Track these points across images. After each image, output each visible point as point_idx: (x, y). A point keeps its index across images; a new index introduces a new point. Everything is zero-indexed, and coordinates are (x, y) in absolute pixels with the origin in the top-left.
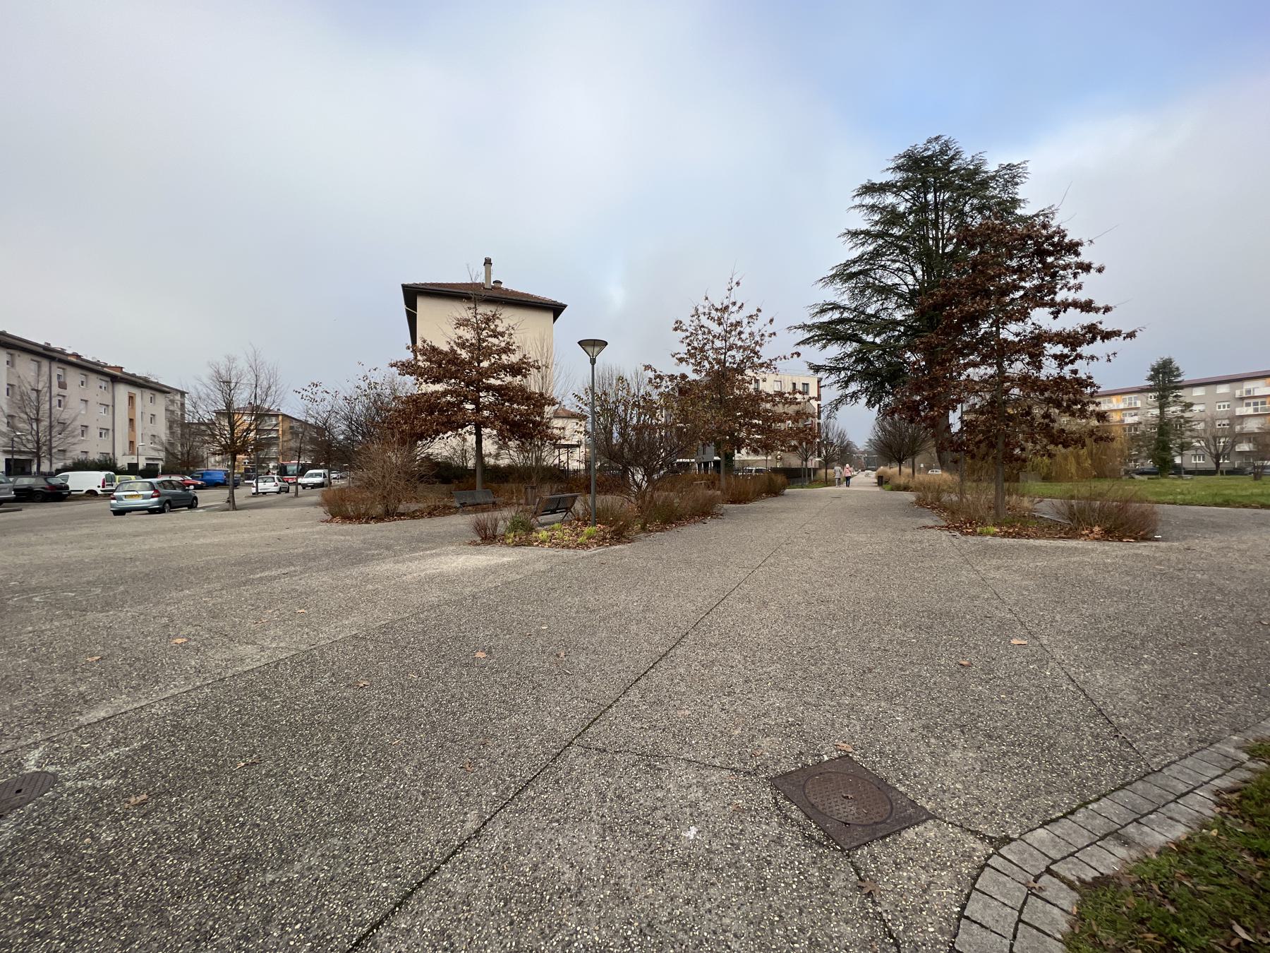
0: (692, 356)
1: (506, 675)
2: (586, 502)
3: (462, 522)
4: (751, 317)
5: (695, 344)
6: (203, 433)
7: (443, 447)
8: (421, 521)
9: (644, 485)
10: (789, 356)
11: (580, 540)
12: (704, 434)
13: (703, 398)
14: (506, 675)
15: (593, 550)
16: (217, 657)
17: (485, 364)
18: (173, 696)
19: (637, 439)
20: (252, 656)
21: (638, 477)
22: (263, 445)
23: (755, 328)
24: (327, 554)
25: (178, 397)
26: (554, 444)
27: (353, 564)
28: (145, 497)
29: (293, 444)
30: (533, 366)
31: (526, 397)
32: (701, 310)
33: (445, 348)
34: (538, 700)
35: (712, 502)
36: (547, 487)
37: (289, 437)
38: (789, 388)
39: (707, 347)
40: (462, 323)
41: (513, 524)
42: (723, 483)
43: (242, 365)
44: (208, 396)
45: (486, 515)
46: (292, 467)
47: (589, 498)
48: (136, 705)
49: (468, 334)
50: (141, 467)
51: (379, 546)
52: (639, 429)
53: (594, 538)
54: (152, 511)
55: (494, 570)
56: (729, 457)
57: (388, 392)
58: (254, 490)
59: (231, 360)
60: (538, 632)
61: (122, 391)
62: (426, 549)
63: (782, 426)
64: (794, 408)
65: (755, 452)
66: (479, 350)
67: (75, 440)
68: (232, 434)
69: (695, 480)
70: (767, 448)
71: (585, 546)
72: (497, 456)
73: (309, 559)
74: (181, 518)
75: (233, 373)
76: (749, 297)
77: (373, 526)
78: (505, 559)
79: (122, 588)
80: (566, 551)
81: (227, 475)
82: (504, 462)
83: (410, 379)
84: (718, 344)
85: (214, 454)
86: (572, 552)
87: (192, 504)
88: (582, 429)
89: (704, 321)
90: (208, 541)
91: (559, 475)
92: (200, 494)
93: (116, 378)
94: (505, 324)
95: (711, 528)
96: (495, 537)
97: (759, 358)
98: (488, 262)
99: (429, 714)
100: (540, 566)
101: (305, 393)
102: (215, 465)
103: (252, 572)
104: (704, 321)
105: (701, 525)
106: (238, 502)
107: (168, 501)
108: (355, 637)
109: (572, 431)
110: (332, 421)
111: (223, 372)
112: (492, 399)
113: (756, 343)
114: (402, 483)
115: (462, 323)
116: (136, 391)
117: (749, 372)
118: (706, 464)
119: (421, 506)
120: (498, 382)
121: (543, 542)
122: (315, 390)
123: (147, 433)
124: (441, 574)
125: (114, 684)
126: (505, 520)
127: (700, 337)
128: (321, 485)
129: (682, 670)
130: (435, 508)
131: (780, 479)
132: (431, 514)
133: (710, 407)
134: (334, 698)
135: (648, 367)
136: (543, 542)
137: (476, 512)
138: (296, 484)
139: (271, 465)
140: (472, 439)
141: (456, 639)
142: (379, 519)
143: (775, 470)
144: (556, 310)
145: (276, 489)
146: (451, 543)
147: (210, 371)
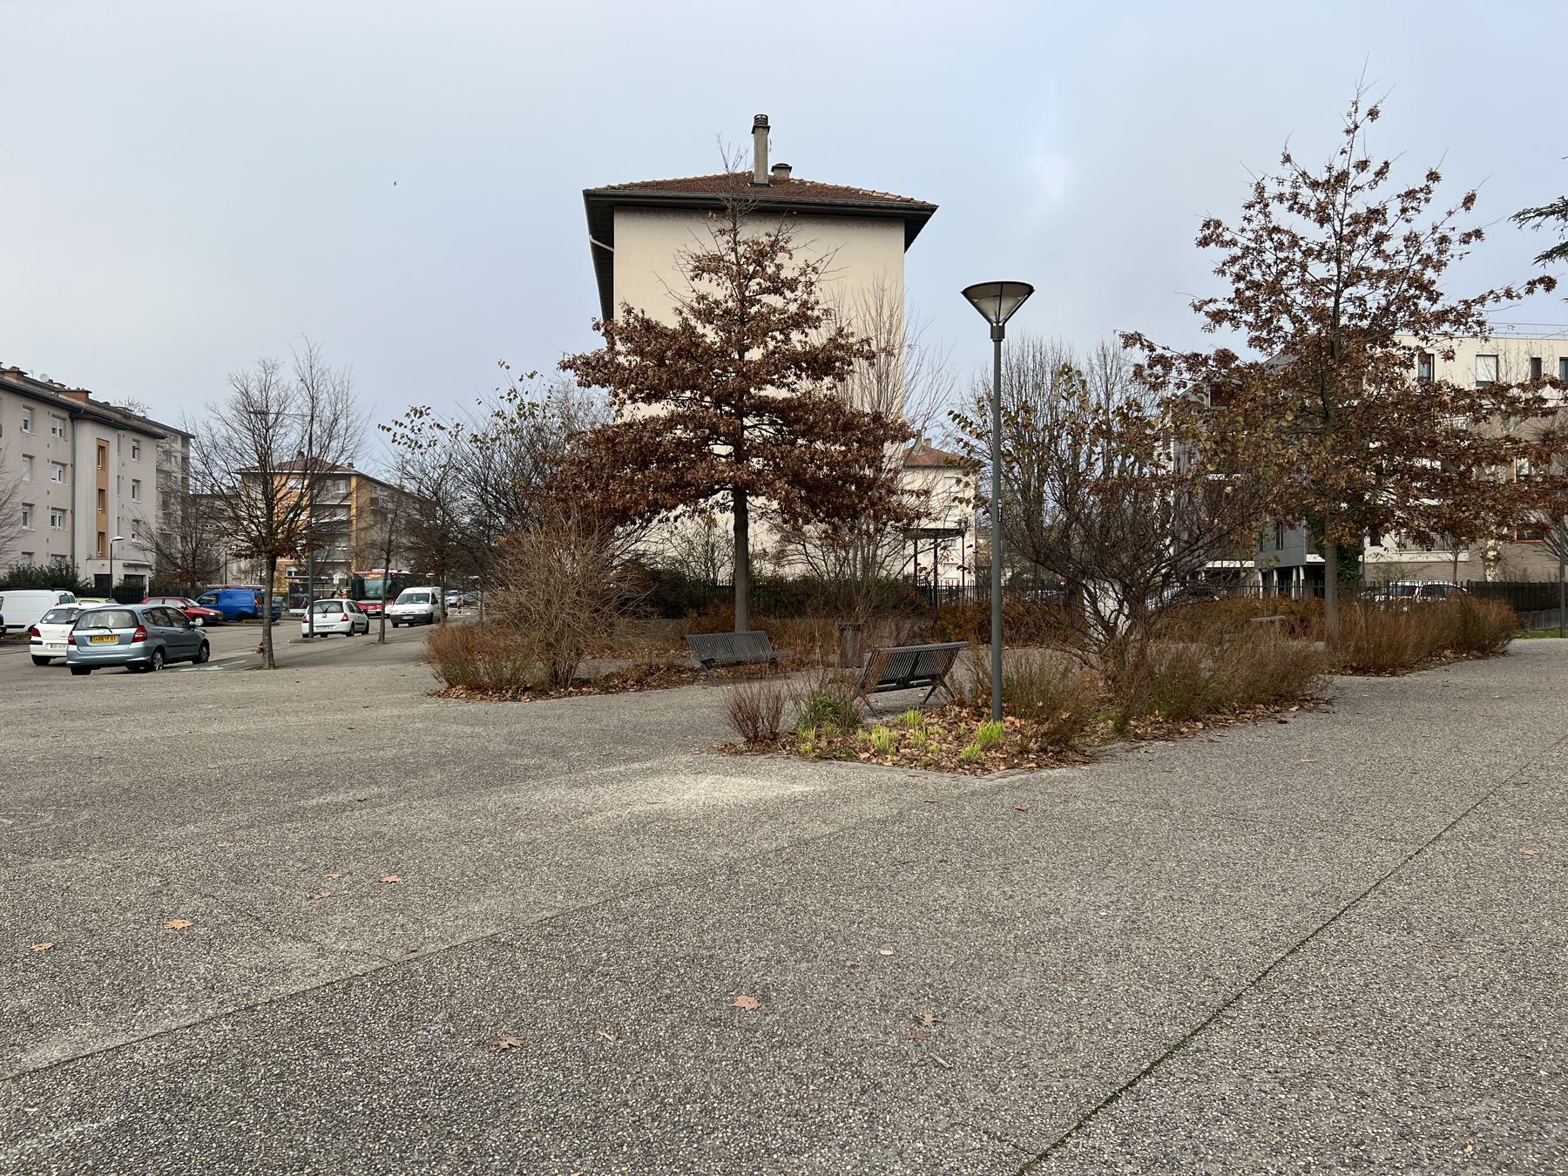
0: (1246, 304)
1: (800, 1053)
2: (978, 663)
3: (706, 702)
4: (1411, 194)
5: (1257, 275)
6: (216, 515)
7: (667, 539)
8: (623, 697)
9: (1123, 624)
10: (1519, 287)
11: (966, 751)
12: (1279, 498)
13: (1278, 409)
14: (800, 1053)
15: (999, 778)
16: (241, 961)
17: (755, 354)
18: (169, 1032)
19: (1106, 515)
20: (303, 965)
21: (1108, 605)
22: (321, 537)
23: (1421, 223)
24: (440, 762)
25: (178, 446)
26: (906, 530)
27: (488, 785)
28: (123, 640)
29: (378, 535)
30: (859, 353)
31: (843, 423)
32: (1272, 189)
33: (672, 322)
34: (872, 1118)
35: (1302, 667)
36: (887, 627)
37: (369, 520)
38: (1522, 373)
39: (1287, 281)
40: (706, 266)
41: (814, 709)
42: (1332, 621)
43: (288, 377)
44: (229, 440)
45: (756, 686)
46: (375, 580)
47: (987, 654)
48: (109, 1043)
49: (718, 290)
50: (116, 582)
51: (538, 749)
52: (1109, 490)
53: (998, 747)
54: (134, 667)
55: (769, 812)
56: (1348, 556)
57: (557, 421)
58: (305, 628)
59: (269, 368)
60: (872, 961)
61: (88, 436)
62: (632, 759)
63: (1502, 473)
64: (1537, 424)
65: (1423, 540)
66: (742, 322)
67: (13, 531)
68: (270, 515)
69: (1255, 612)
70: (1457, 531)
71: (978, 766)
72: (779, 557)
73: (405, 773)
74: (180, 681)
75: (273, 394)
76: (1402, 149)
77: (528, 706)
78: (798, 788)
79: (85, 815)
80: (932, 777)
81: (260, 598)
82: (794, 570)
83: (600, 395)
84: (1318, 270)
85: (238, 556)
86: (947, 778)
87: (199, 654)
88: (970, 493)
89: (1280, 215)
90: (228, 729)
91: (917, 599)
92: (214, 635)
93: (78, 411)
94: (799, 260)
95: (1299, 732)
96: (775, 737)
97: (1434, 298)
98: (761, 125)
99: (638, 1124)
100: (875, 808)
101: (399, 430)
102: (239, 576)
103: (303, 793)
104: (1280, 215)
105: (1273, 728)
106: (278, 651)
107: (160, 649)
108: (492, 940)
109: (946, 498)
110: (449, 486)
111: (255, 393)
112: (769, 431)
113: (1426, 261)
114: (585, 616)
115: (706, 266)
116: (110, 436)
117: (1405, 338)
118: (1285, 574)
119: (623, 664)
120: (783, 394)
121: (880, 753)
122: (418, 422)
123: (121, 518)
124: (662, 816)
125: (72, 997)
126: (796, 699)
127: (1269, 257)
128: (427, 619)
129: (1226, 1088)
130: (651, 670)
131: (1494, 612)
132: (641, 684)
133: (1295, 430)
134: (452, 1067)
135: (1132, 340)
136: (880, 753)
137: (735, 680)
138: (382, 616)
139: (337, 578)
140: (726, 521)
141: (693, 960)
142: (539, 691)
143: (1481, 590)
144: (911, 219)
145: (345, 626)
146: (684, 748)
147: (233, 393)
